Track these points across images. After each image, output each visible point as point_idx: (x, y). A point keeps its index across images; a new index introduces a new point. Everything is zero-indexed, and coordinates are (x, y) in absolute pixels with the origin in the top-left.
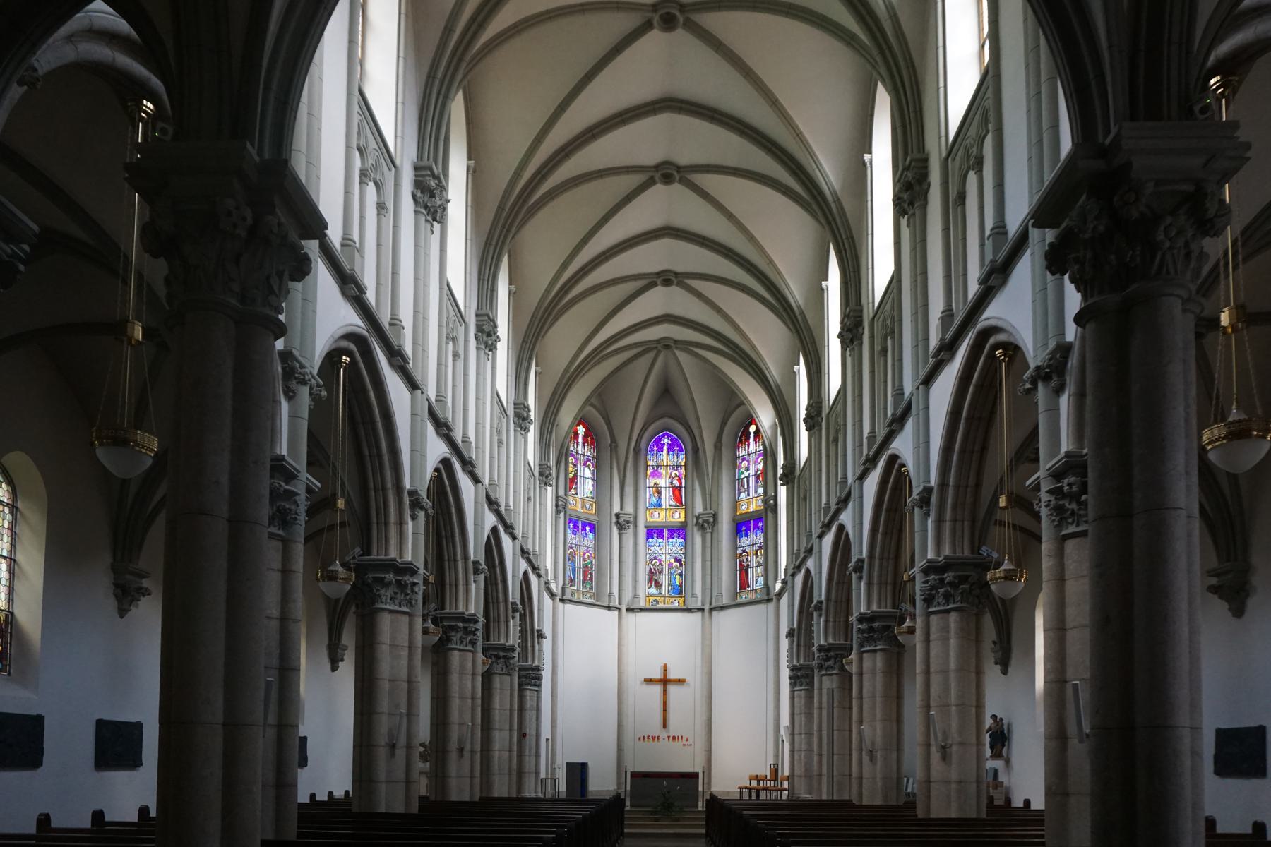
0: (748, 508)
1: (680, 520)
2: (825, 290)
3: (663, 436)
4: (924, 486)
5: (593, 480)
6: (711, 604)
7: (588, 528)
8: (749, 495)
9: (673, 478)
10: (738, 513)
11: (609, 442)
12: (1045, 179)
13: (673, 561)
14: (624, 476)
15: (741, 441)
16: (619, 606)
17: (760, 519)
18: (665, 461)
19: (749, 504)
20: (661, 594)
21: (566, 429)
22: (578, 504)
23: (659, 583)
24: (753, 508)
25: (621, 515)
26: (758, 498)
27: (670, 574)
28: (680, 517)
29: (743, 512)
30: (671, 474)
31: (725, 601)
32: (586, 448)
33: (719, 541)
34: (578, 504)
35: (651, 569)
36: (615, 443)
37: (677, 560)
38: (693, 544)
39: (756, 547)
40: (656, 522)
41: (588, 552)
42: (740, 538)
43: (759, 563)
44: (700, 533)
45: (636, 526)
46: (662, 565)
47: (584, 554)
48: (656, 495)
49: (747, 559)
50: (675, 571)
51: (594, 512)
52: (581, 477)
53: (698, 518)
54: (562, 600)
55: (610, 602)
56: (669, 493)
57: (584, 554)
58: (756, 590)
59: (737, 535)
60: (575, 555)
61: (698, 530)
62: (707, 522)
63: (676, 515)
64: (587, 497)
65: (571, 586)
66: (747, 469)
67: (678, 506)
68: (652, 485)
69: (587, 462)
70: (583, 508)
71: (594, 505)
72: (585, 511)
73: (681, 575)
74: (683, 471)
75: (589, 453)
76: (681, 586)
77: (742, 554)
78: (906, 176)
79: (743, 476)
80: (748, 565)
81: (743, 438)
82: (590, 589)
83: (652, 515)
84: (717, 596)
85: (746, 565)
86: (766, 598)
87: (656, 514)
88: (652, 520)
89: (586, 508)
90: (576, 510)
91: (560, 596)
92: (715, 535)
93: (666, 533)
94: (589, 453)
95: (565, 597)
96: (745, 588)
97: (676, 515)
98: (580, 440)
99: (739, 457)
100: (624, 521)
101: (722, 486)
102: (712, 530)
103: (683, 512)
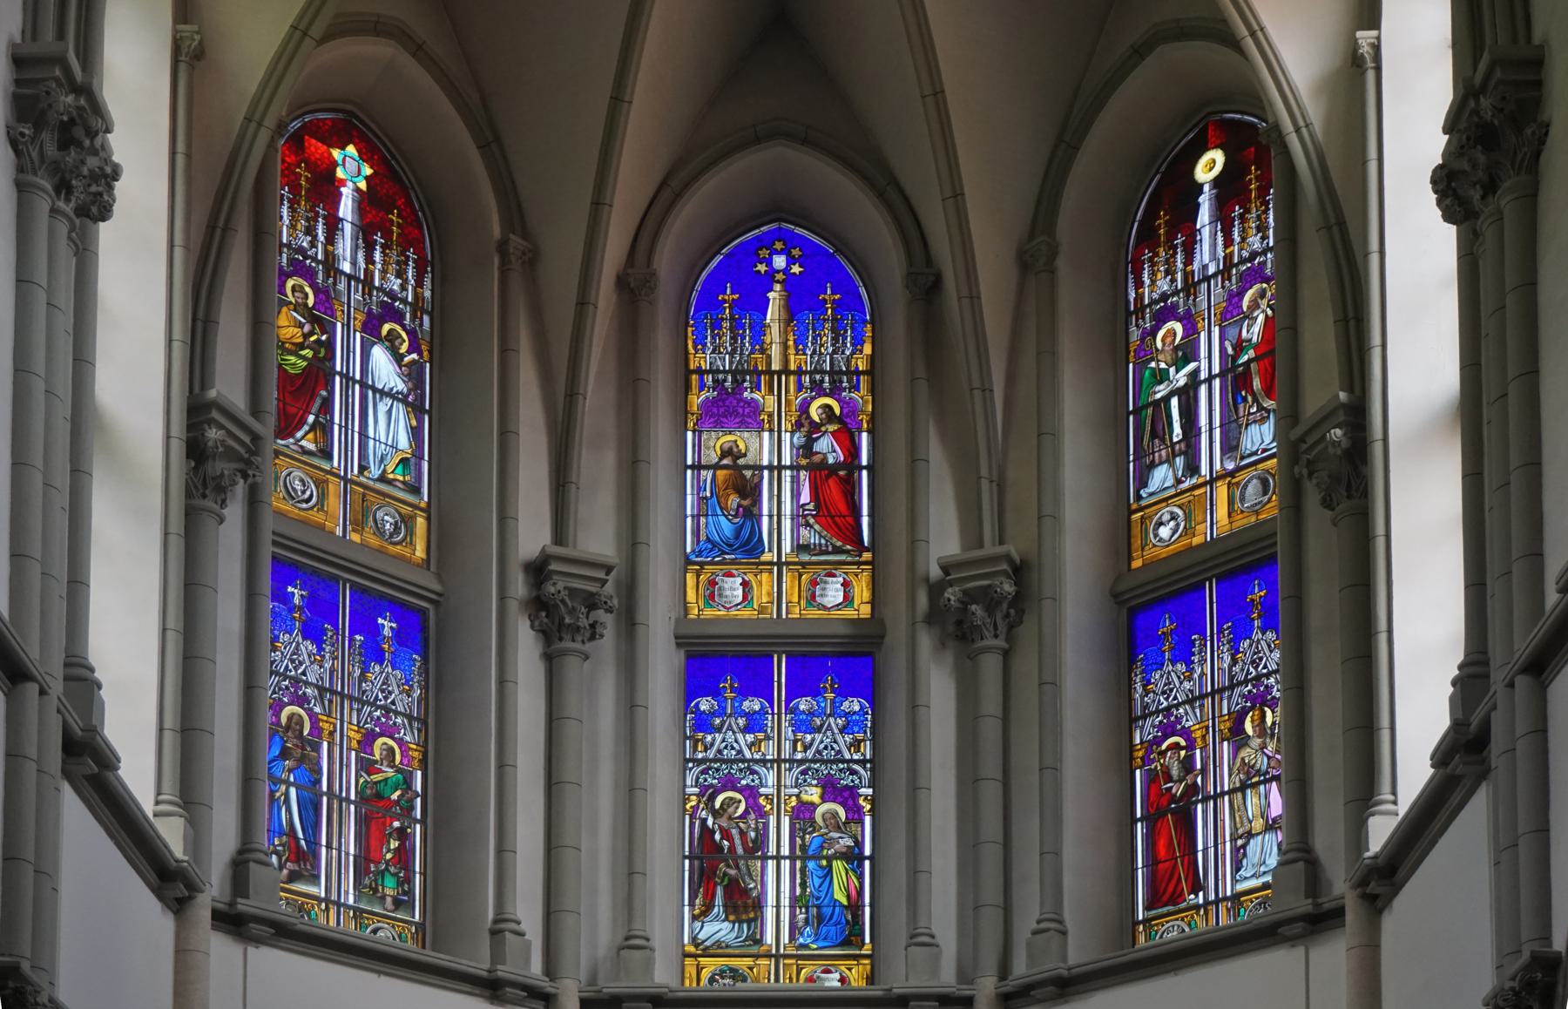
0: (1189, 531)
1: (849, 613)
2: (1370, 64)
3: (766, 242)
4: (1532, 952)
5: (416, 408)
6: (1004, 972)
7: (387, 625)
8: (1192, 468)
9: (815, 427)
10: (1137, 564)
11: (496, 231)
12: (1516, 648)
13: (813, 794)
14: (572, 395)
15: (1148, 238)
16: (546, 985)
17: (1263, 567)
18: (775, 351)
19: (1192, 504)
20: (759, 942)
21: (253, 88)
22: (334, 503)
23: (746, 892)
24: (1220, 518)
25: (554, 566)
26: (1242, 477)
27: (800, 854)
28: (848, 599)
29: (1164, 553)
30: (804, 408)
31: (1078, 953)
32: (378, 256)
33: (1050, 685)
34: (334, 503)
35: (707, 832)
36: (525, 235)
37: (831, 790)
38: (913, 707)
39: (1237, 700)
40: (735, 620)
41: (389, 732)
42: (1147, 672)
43: (1248, 769)
44: (949, 658)
45: (630, 621)
46: (762, 814)
47: (368, 740)
48: (733, 501)
49: (1188, 765)
50: (826, 842)
51: (420, 552)
52: (347, 378)
53: (935, 590)
54: (231, 922)
55: (497, 955)
56: (796, 494)
57: (368, 740)
58: (1237, 897)
59: (1132, 660)
60: (316, 729)
61: (942, 645)
62: (989, 598)
63: (833, 593)
64: (382, 478)
65: (293, 877)
66: (1187, 353)
67: (837, 551)
68: (712, 457)
69: (383, 319)
70: (359, 526)
71: (421, 522)
72: (374, 541)
73: (853, 857)
74: (862, 397)
75: (395, 284)
76: (855, 906)
77: (1158, 741)
78: (1476, 112)
79: (1161, 391)
80: (1192, 789)
81: (1162, 219)
82: (398, 904)
83: (711, 593)
84: (1035, 933)
85: (1178, 789)
86: (1304, 906)
87: (732, 588)
88: (709, 613)
89: (379, 531)
90: (322, 527)
91: (215, 886)
92: (1026, 665)
93: (780, 671)
94: (395, 284)
95: (243, 906)
96: (1177, 897)
97: (833, 593)
98: (346, 209)
99: (1140, 309)
100: (572, 592)
101: (1056, 435)
102: (1009, 638)
103: (865, 577)
